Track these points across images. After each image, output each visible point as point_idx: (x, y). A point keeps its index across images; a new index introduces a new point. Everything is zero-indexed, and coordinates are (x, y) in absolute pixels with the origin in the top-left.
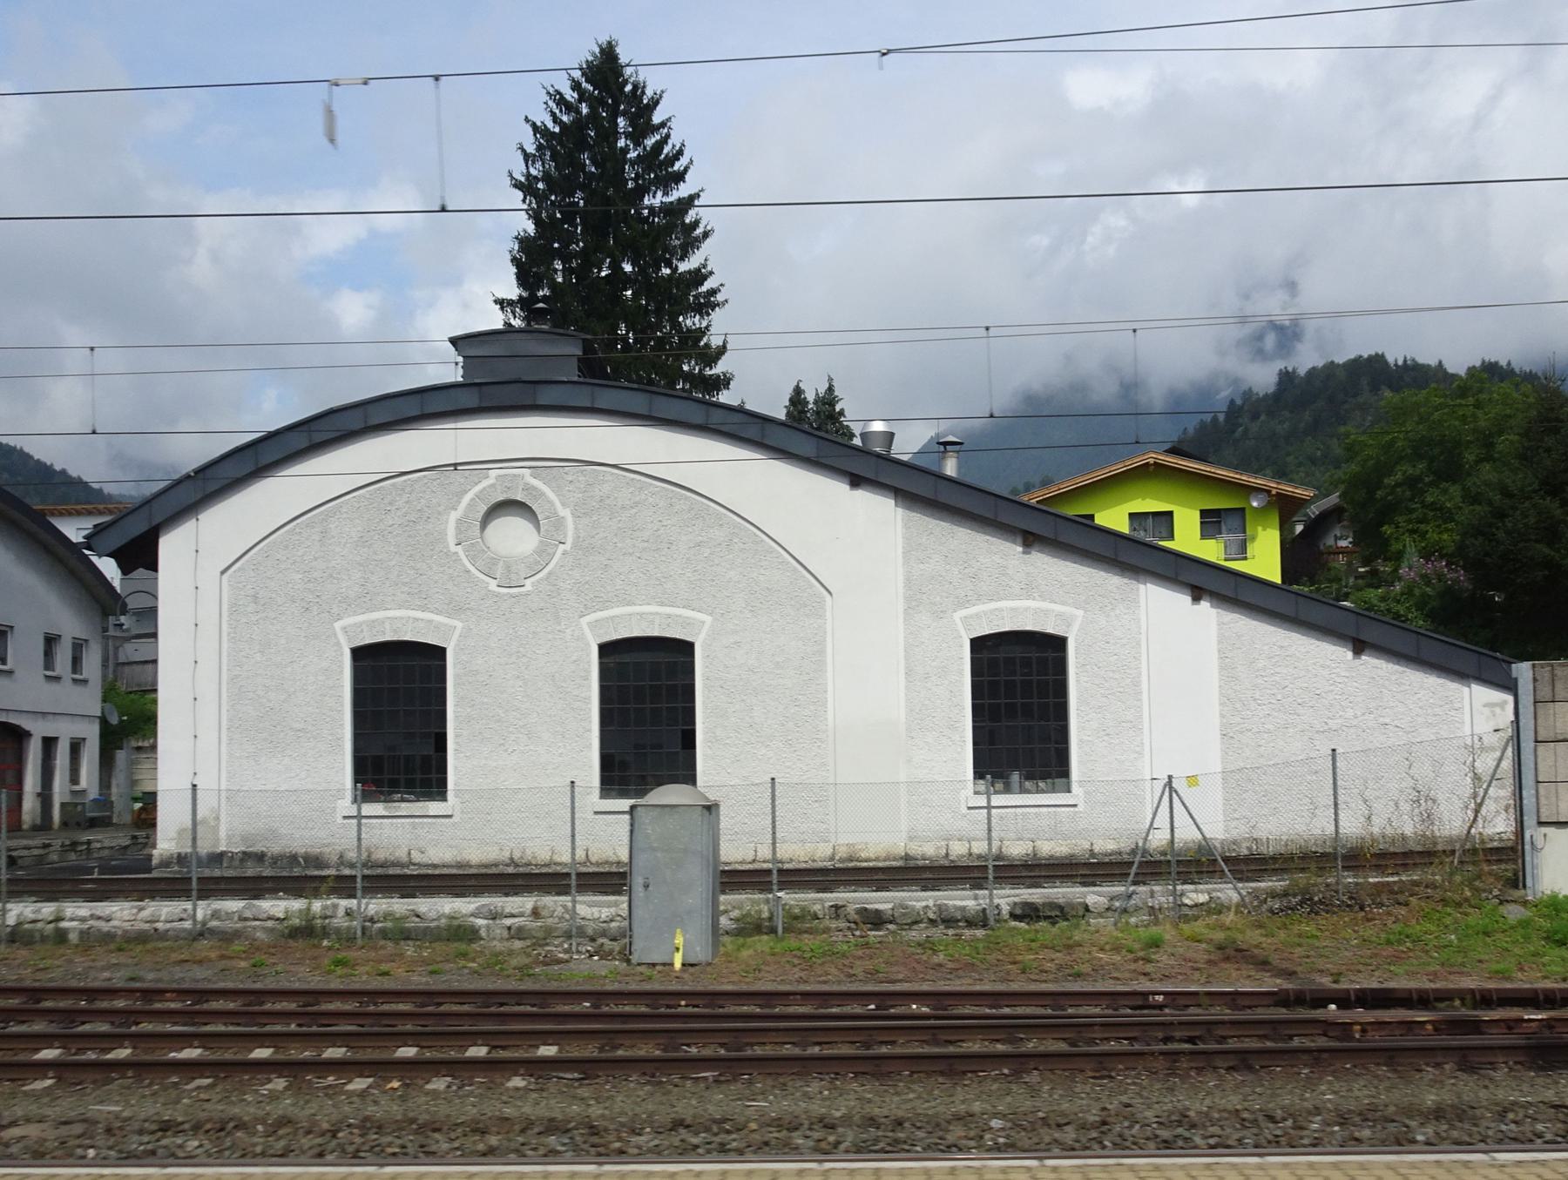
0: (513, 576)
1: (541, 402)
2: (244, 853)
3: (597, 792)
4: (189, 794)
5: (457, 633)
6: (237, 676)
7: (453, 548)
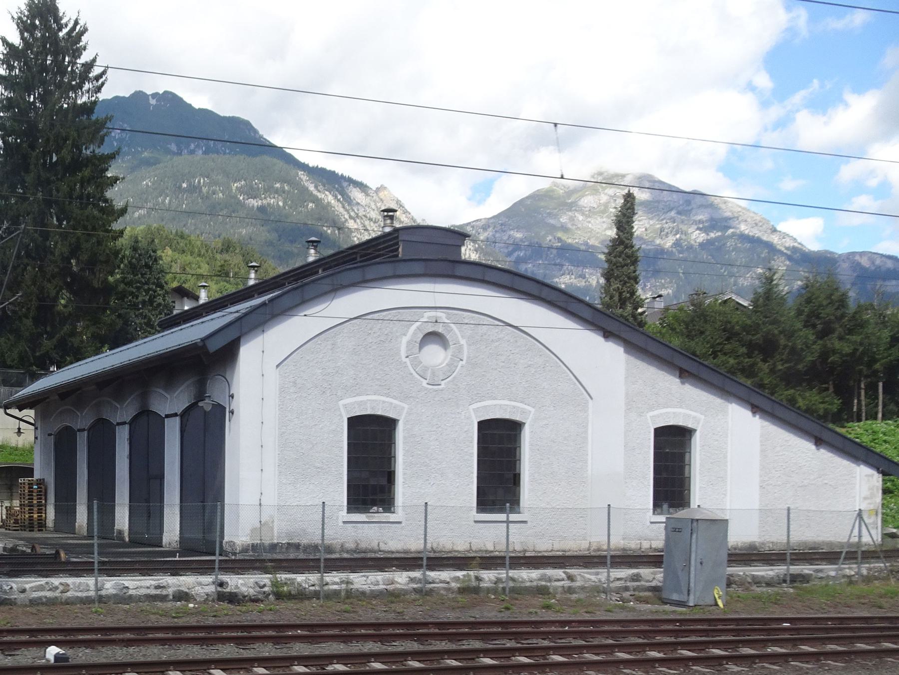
0: (436, 379)
1: (457, 274)
2: (288, 544)
3: (475, 509)
4: (786, 512)
5: (405, 411)
6: (284, 433)
7: (404, 360)
